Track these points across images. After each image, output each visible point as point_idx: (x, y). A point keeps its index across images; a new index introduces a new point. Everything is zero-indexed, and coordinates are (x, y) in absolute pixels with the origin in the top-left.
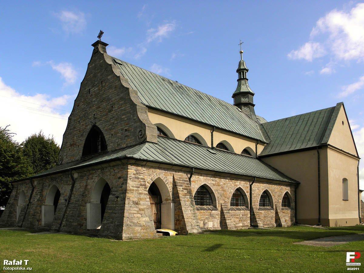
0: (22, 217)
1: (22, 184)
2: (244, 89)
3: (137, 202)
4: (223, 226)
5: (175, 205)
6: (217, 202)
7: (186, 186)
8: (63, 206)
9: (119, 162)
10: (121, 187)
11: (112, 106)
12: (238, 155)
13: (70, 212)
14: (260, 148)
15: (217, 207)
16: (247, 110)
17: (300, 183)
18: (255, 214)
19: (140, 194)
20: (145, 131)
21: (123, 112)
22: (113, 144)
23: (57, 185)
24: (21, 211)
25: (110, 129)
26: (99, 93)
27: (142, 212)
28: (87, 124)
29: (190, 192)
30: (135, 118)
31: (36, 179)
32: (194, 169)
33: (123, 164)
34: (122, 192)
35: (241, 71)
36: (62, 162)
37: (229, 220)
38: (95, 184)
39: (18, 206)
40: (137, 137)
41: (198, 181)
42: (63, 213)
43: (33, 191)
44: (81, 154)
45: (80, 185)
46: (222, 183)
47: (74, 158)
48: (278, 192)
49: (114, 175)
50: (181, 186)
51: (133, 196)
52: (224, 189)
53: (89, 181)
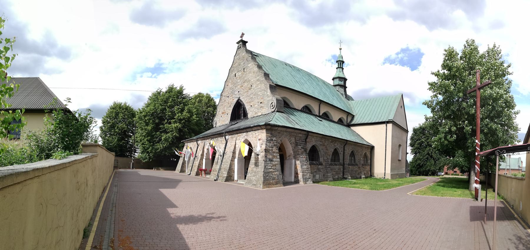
19: (274, 152)
26: (242, 76)
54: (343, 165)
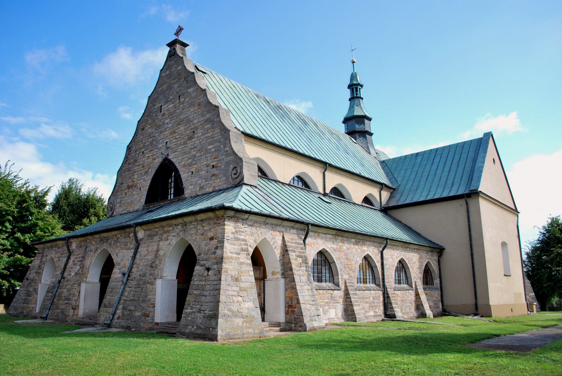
0: (48, 303)
1: (52, 247)
2: (357, 112)
3: (236, 277)
4: (349, 315)
5: (285, 282)
6: (340, 276)
7: (300, 252)
8: (118, 283)
9: (211, 215)
10: (214, 253)
11: (194, 132)
12: (358, 205)
13: (129, 293)
15: (340, 285)
17: (444, 249)
18: (390, 296)
19: (242, 264)
20: (241, 168)
21: (210, 140)
22: (193, 186)
23: (110, 250)
24: (48, 292)
25: (190, 165)
27: (243, 294)
28: (155, 156)
29: (305, 261)
30: (227, 149)
31: (76, 239)
32: (310, 226)
33: (218, 218)
34: (215, 261)
35: (354, 88)
36: (113, 213)
37: (357, 305)
38: (171, 248)
41: (316, 244)
42: (119, 296)
43: (69, 258)
44: (143, 200)
45: (148, 250)
47: (132, 206)
48: (415, 261)
49: (202, 235)
51: (231, 268)
52: (348, 257)
53: (161, 243)
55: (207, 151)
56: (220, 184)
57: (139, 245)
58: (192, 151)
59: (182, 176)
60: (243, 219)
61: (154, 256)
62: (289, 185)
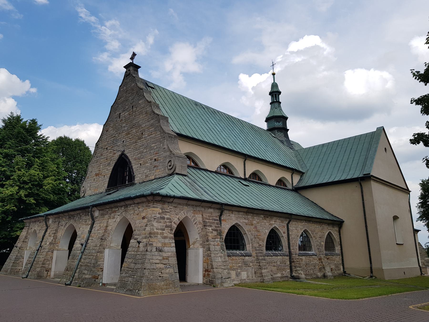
0: (29, 266)
1: (35, 222)
9: (144, 199)
14: (296, 179)
16: (280, 135)
17: (343, 222)
19: (165, 238)
22: (141, 175)
23: (75, 225)
29: (220, 234)
34: (145, 236)
39: (26, 249)
40: (167, 168)
46: (255, 222)
50: (211, 226)
54: (290, 254)
55: (151, 148)
56: (160, 173)
57: (94, 222)
58: (141, 148)
59: (134, 167)
60: (169, 202)
61: (104, 231)
62: (216, 172)
